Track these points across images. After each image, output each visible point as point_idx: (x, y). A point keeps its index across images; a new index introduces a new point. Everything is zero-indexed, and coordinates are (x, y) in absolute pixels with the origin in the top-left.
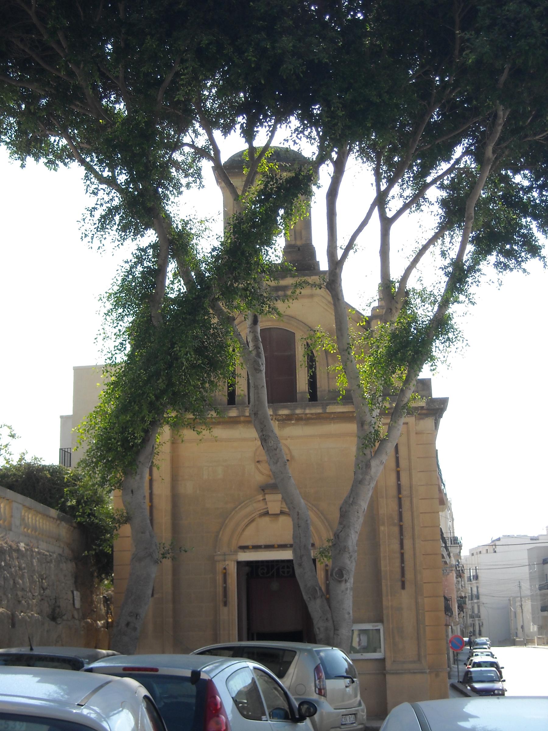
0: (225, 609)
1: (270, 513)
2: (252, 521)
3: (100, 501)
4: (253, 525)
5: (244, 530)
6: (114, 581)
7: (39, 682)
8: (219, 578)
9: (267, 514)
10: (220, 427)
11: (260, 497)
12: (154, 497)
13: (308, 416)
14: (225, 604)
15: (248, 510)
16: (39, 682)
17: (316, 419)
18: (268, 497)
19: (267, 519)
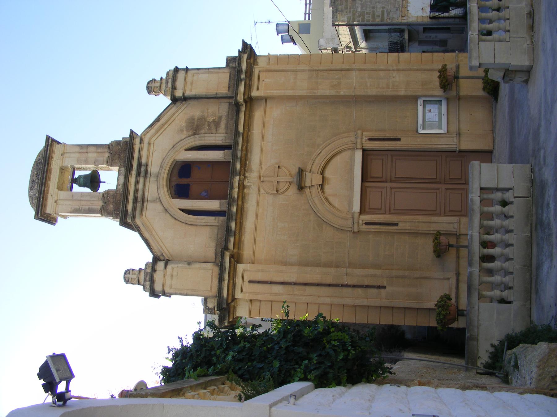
0: (400, 224)
1: (321, 183)
2: (327, 199)
3: (320, 332)
4: (330, 199)
5: (334, 207)
6: (58, 202)
7: (239, 50)
8: (373, 228)
9: (322, 186)
10: (244, 223)
11: (307, 191)
12: (298, 282)
13: (244, 149)
14: (396, 224)
15: (317, 201)
16: (239, 50)
17: (247, 143)
18: (308, 183)
19: (327, 188)
